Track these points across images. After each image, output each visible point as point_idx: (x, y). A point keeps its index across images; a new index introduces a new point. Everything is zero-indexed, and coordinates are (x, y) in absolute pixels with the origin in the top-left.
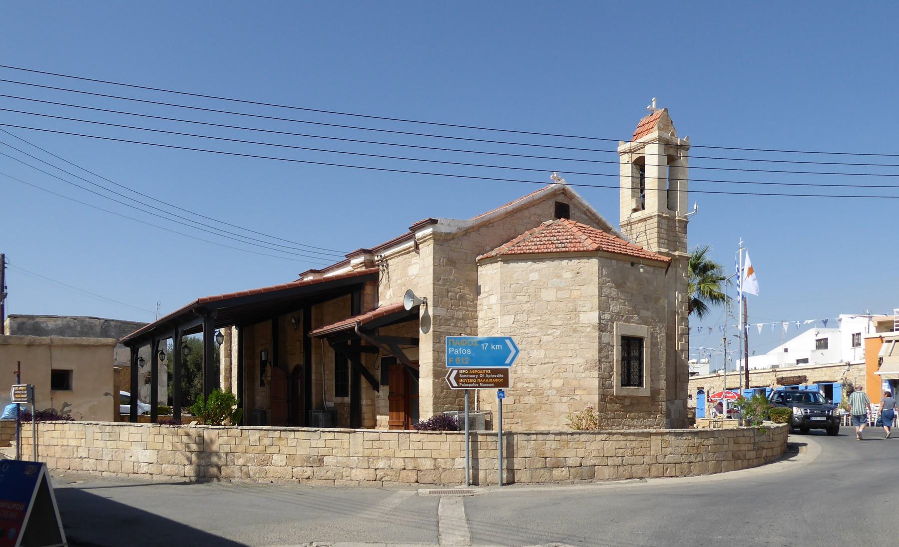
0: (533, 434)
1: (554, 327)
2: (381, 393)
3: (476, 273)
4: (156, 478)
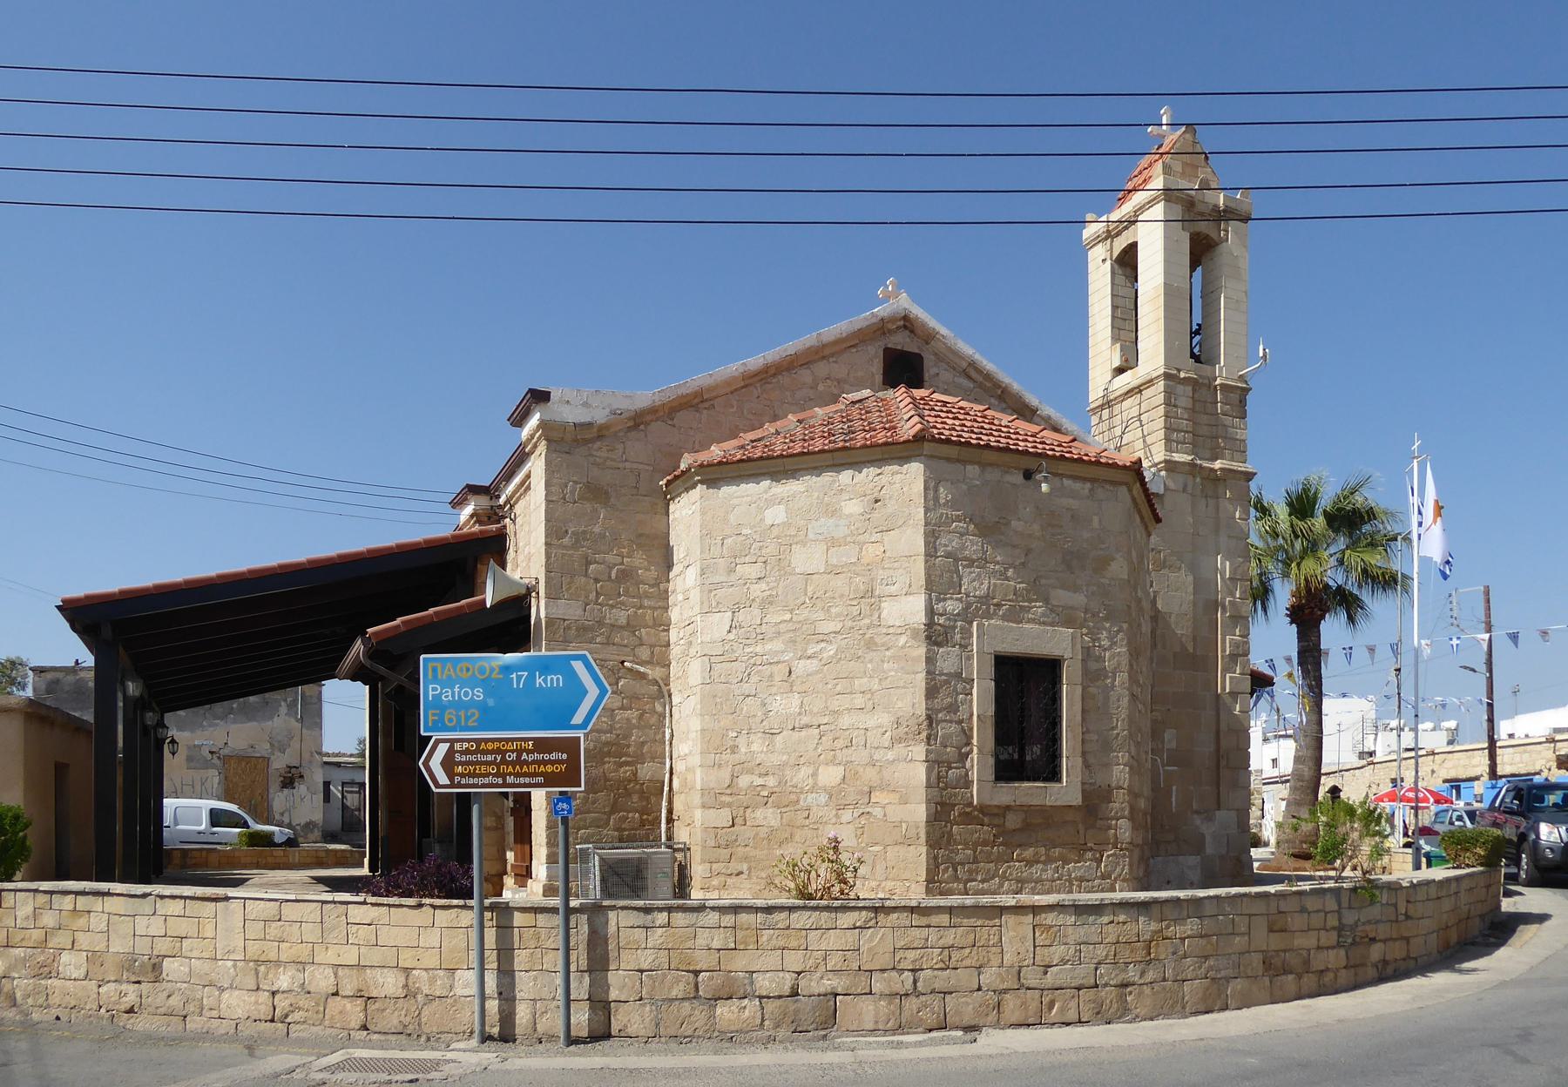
1: (821, 637)
3: (666, 517)
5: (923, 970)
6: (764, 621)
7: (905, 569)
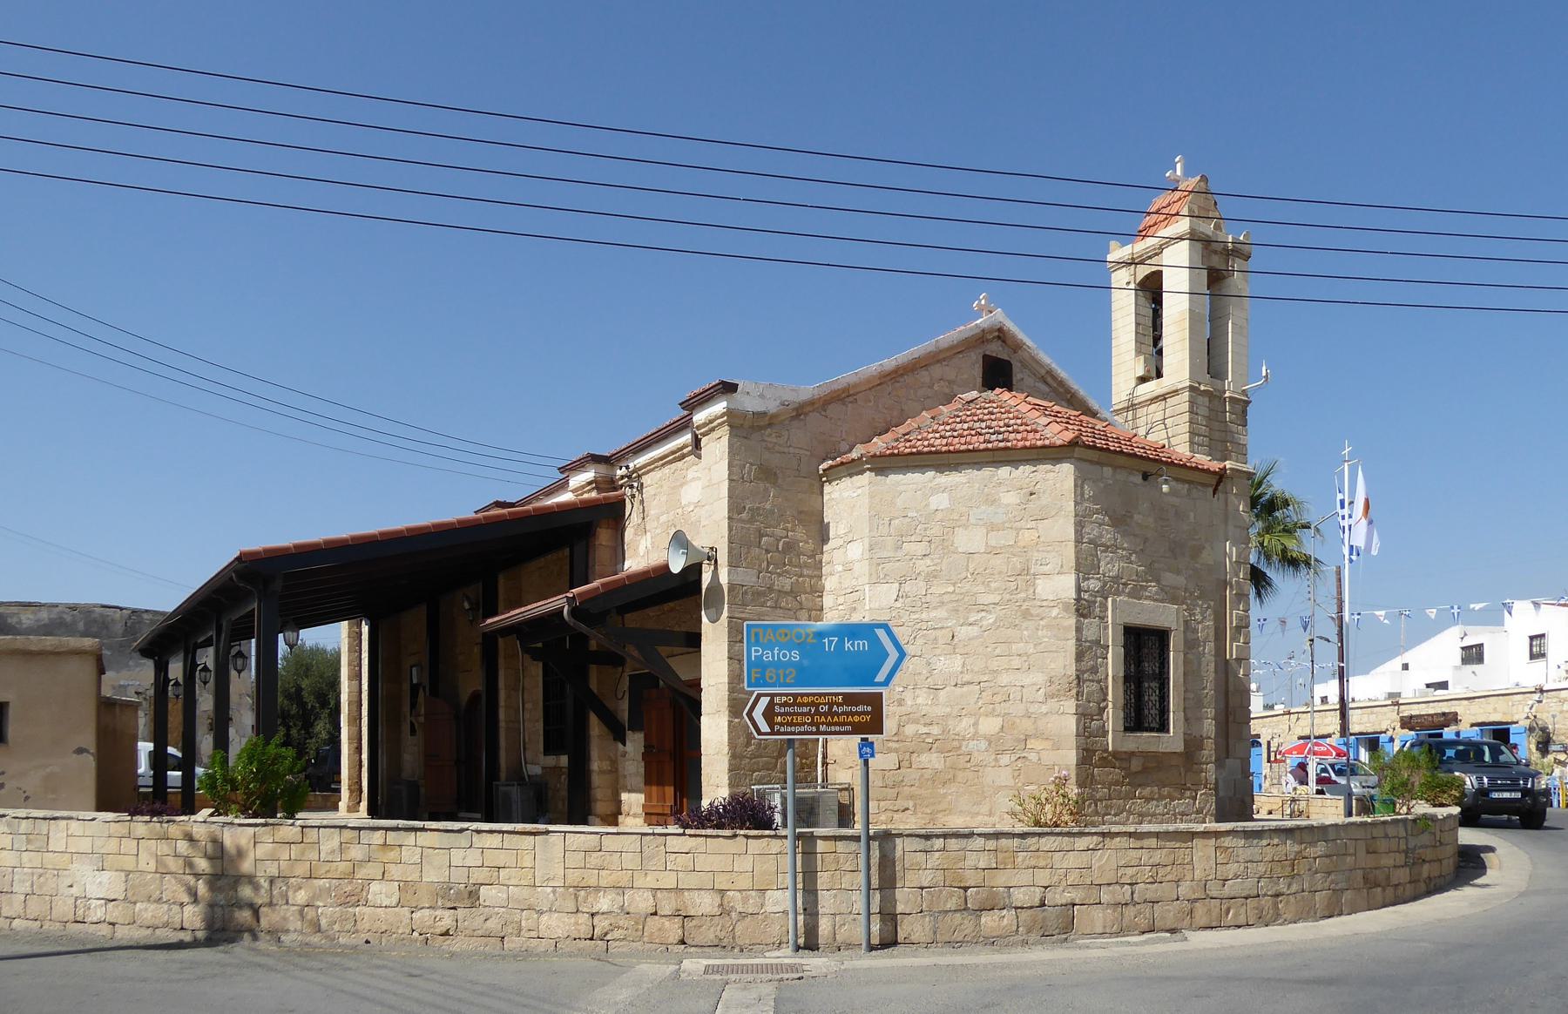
0: (938, 836)
2: (629, 747)
3: (821, 497)
4: (124, 934)
5: (1137, 884)
6: (929, 591)
7: (1057, 552)
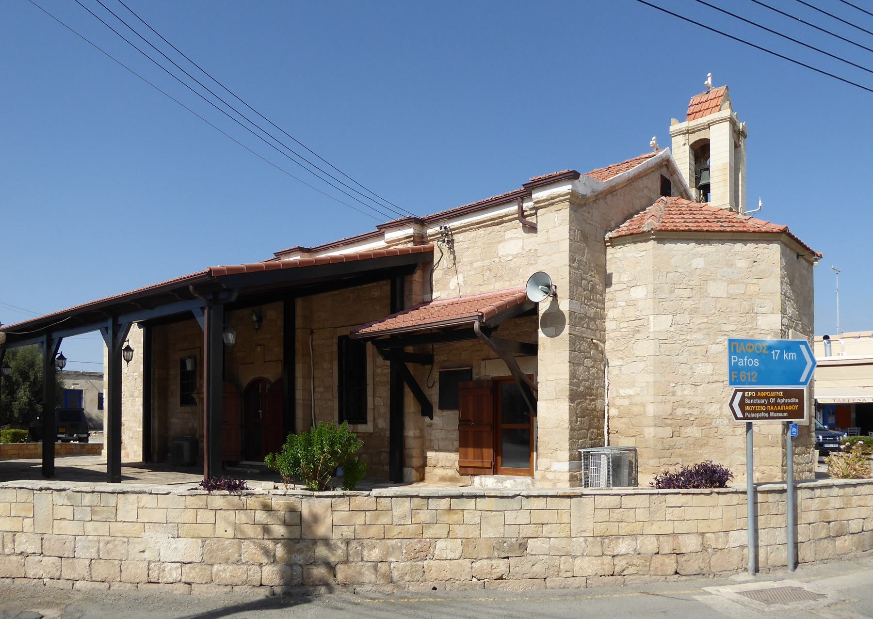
1: (725, 333)
6: (692, 321)
